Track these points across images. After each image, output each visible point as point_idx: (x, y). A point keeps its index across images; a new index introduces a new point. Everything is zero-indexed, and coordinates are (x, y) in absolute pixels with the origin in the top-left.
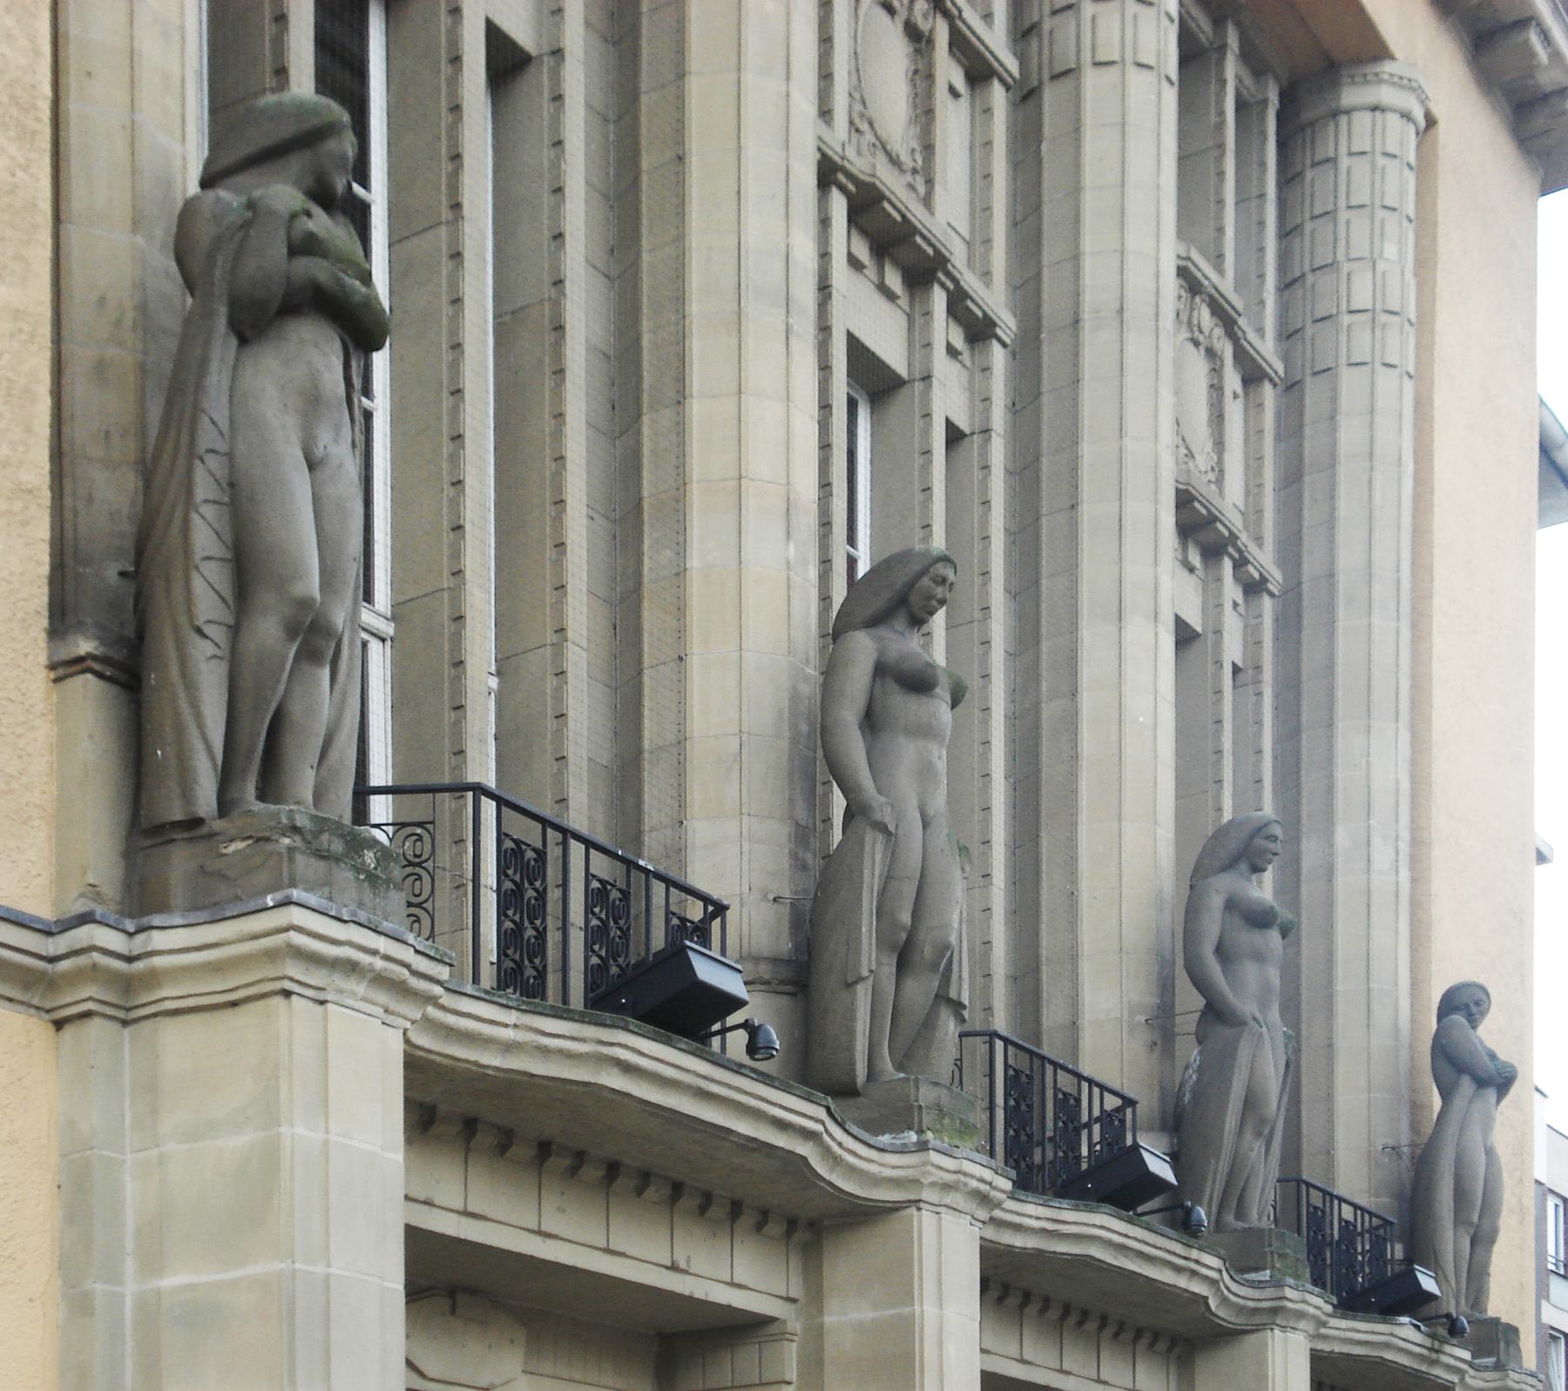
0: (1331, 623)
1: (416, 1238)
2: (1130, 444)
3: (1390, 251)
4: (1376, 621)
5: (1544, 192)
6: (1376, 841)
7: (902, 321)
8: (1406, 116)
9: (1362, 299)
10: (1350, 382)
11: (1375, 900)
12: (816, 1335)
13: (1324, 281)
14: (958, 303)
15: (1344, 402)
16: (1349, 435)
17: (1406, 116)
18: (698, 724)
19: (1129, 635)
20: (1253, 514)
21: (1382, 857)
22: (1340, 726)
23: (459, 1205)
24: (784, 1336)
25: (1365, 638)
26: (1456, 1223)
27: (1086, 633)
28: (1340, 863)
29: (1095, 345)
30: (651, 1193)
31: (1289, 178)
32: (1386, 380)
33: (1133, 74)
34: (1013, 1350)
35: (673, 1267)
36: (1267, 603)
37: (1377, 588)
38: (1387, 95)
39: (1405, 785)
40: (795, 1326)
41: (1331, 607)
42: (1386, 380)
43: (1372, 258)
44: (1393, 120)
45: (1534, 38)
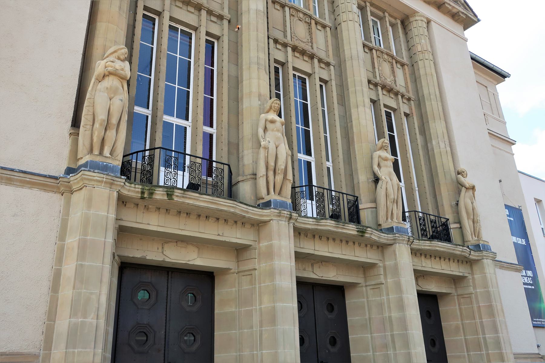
0: (425, 104)
1: (415, 270)
2: (356, 78)
3: (423, 41)
4: (433, 103)
5: (465, 29)
6: (440, 143)
7: (310, 65)
8: (422, 20)
9: (420, 49)
10: (420, 63)
11: (442, 154)
12: (473, 278)
13: (413, 48)
14: (320, 61)
15: (420, 67)
16: (422, 72)
17: (422, 20)
18: (245, 134)
19: (359, 110)
20: (407, 88)
21: (442, 145)
22: (430, 122)
23: (157, 224)
24: (255, 249)
25: (432, 106)
26: (468, 219)
27: (352, 111)
28: (434, 148)
29: (348, 64)
30: (210, 220)
31: (406, 34)
32: (427, 62)
33: (349, 22)
34: (326, 250)
35: (219, 235)
36: (412, 102)
37: (431, 97)
38: (417, 18)
39: (445, 131)
40: (381, 265)
41: (424, 101)
42: (427, 62)
43: (421, 43)
44: (420, 22)
45: (446, 5)
